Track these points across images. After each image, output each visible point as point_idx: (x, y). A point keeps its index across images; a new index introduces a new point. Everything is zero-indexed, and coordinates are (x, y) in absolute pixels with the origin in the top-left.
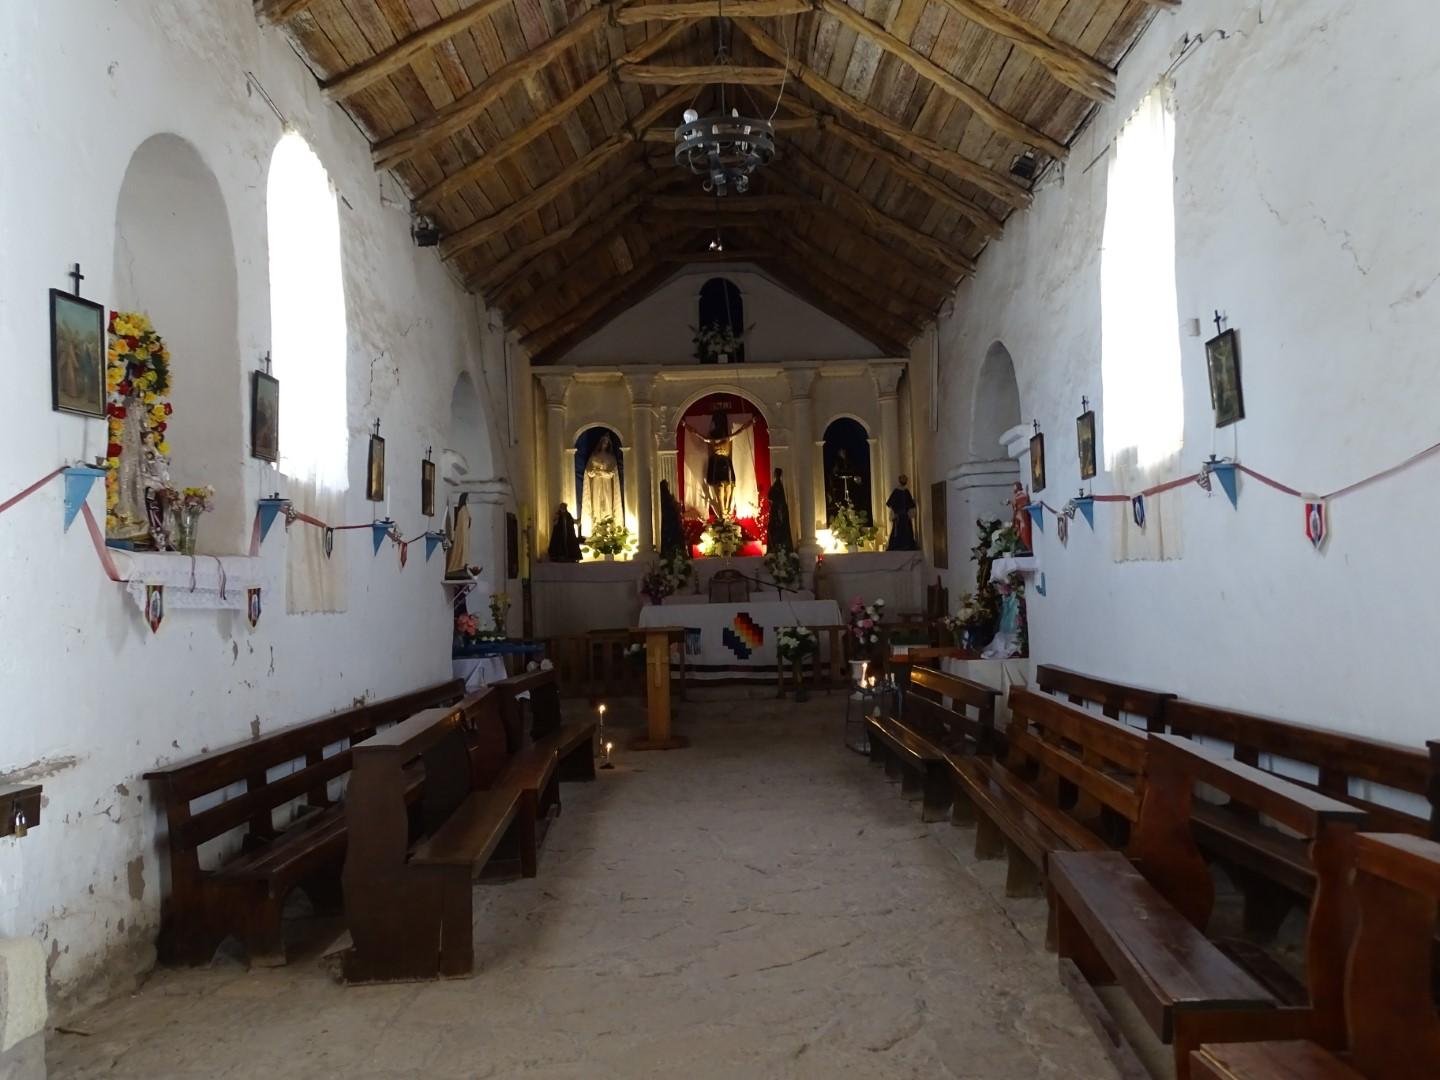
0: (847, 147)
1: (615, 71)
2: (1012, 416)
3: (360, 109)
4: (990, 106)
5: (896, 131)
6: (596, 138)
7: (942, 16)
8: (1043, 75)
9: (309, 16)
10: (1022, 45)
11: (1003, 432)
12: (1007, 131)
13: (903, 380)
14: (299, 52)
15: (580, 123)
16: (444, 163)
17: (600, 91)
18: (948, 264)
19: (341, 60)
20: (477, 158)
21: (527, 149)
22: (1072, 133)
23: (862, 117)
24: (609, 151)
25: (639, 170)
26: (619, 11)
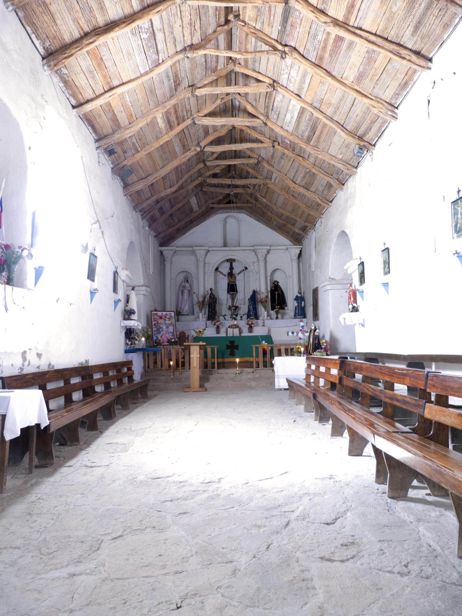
1: (193, 119)
4: (343, 129)
5: (304, 144)
6: (185, 148)
7: (326, 89)
9: (67, 72)
10: (359, 98)
11: (345, 264)
12: (350, 140)
13: (300, 255)
14: (63, 90)
15: (179, 142)
18: (321, 203)
19: (81, 96)
22: (377, 139)
24: (189, 154)
26: (195, 89)
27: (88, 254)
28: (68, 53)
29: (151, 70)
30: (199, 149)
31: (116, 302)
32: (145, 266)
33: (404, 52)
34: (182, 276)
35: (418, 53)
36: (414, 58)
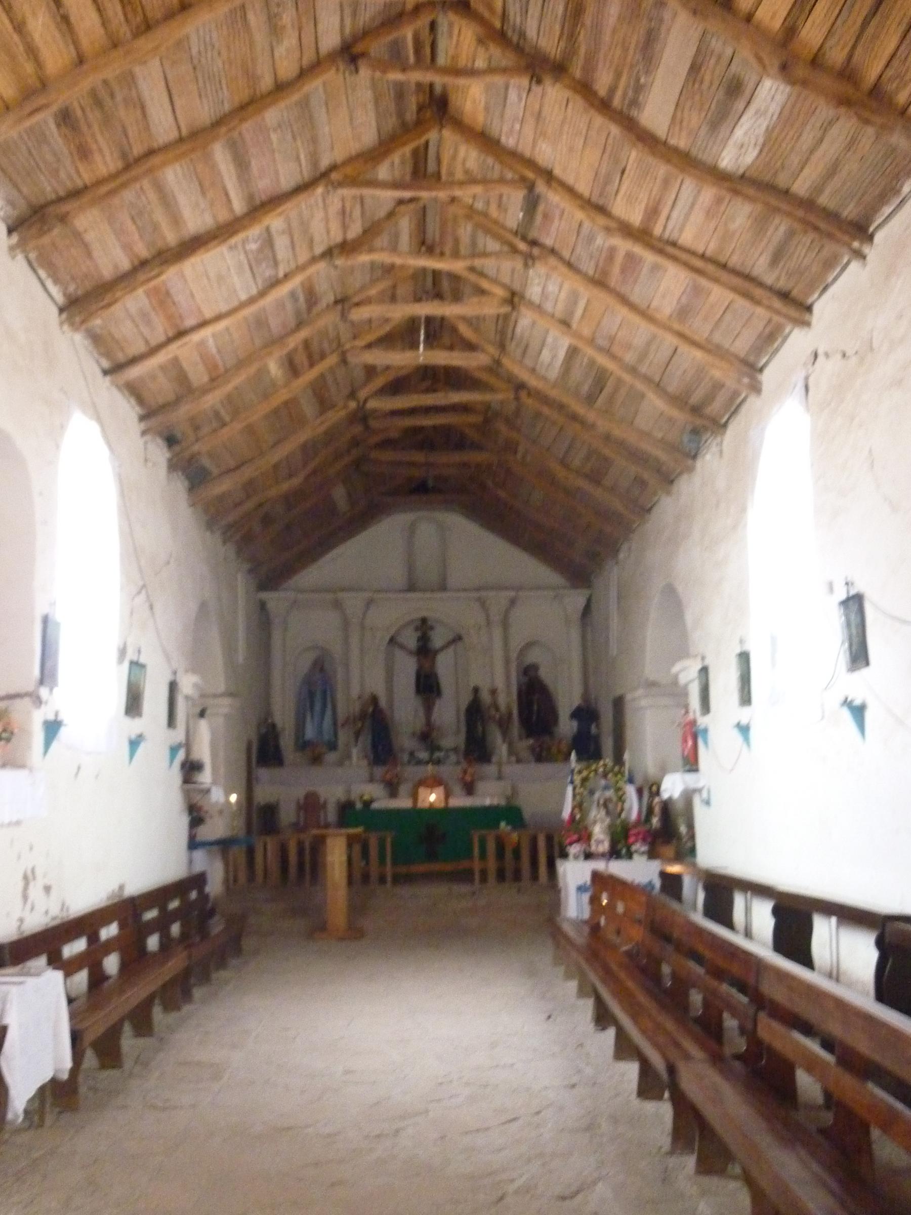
0: (538, 415)
2: (682, 651)
3: (134, 391)
6: (324, 404)
8: (700, 371)
10: (684, 348)
11: (673, 664)
12: (675, 413)
13: (587, 610)
16: (197, 428)
17: (332, 370)
20: (224, 425)
21: (267, 417)
23: (554, 393)
24: (335, 416)
25: (358, 429)
26: (350, 308)
27: (126, 665)
28: (108, 298)
29: (262, 294)
30: (353, 405)
31: (174, 750)
32: (229, 650)
33: (758, 292)
34: (310, 657)
35: (785, 296)
36: (777, 304)
